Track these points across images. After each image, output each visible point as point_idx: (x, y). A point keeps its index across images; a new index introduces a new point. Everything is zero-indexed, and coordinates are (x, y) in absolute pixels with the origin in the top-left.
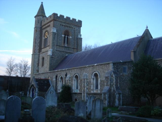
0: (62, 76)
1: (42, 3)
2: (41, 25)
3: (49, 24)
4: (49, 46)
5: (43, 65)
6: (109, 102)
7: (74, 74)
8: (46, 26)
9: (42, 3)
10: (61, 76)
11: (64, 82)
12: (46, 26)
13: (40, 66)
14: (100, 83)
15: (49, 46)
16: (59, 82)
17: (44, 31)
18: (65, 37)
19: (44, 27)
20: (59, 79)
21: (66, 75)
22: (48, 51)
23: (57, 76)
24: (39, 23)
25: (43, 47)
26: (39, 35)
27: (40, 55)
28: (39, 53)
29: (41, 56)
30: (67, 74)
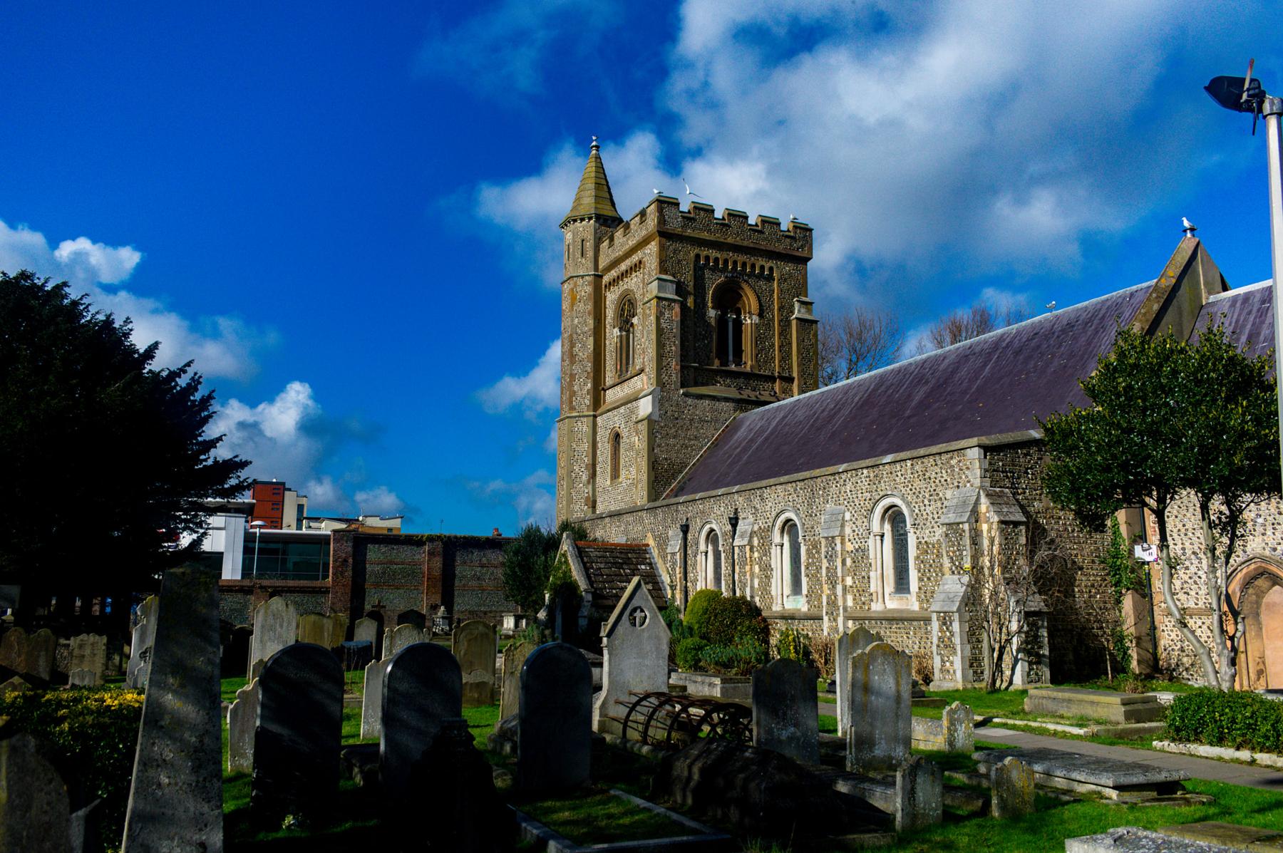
0: (714, 526)
2: (596, 268)
3: (635, 258)
4: (642, 371)
5: (615, 475)
6: (971, 666)
7: (774, 514)
8: (623, 267)
10: (707, 528)
11: (727, 558)
12: (623, 267)
13: (603, 480)
15: (642, 371)
17: (611, 297)
18: (722, 321)
19: (614, 273)
21: (734, 522)
22: (636, 399)
23: (685, 529)
25: (610, 378)
27: (599, 419)
28: (595, 410)
29: (606, 423)
30: (741, 515)
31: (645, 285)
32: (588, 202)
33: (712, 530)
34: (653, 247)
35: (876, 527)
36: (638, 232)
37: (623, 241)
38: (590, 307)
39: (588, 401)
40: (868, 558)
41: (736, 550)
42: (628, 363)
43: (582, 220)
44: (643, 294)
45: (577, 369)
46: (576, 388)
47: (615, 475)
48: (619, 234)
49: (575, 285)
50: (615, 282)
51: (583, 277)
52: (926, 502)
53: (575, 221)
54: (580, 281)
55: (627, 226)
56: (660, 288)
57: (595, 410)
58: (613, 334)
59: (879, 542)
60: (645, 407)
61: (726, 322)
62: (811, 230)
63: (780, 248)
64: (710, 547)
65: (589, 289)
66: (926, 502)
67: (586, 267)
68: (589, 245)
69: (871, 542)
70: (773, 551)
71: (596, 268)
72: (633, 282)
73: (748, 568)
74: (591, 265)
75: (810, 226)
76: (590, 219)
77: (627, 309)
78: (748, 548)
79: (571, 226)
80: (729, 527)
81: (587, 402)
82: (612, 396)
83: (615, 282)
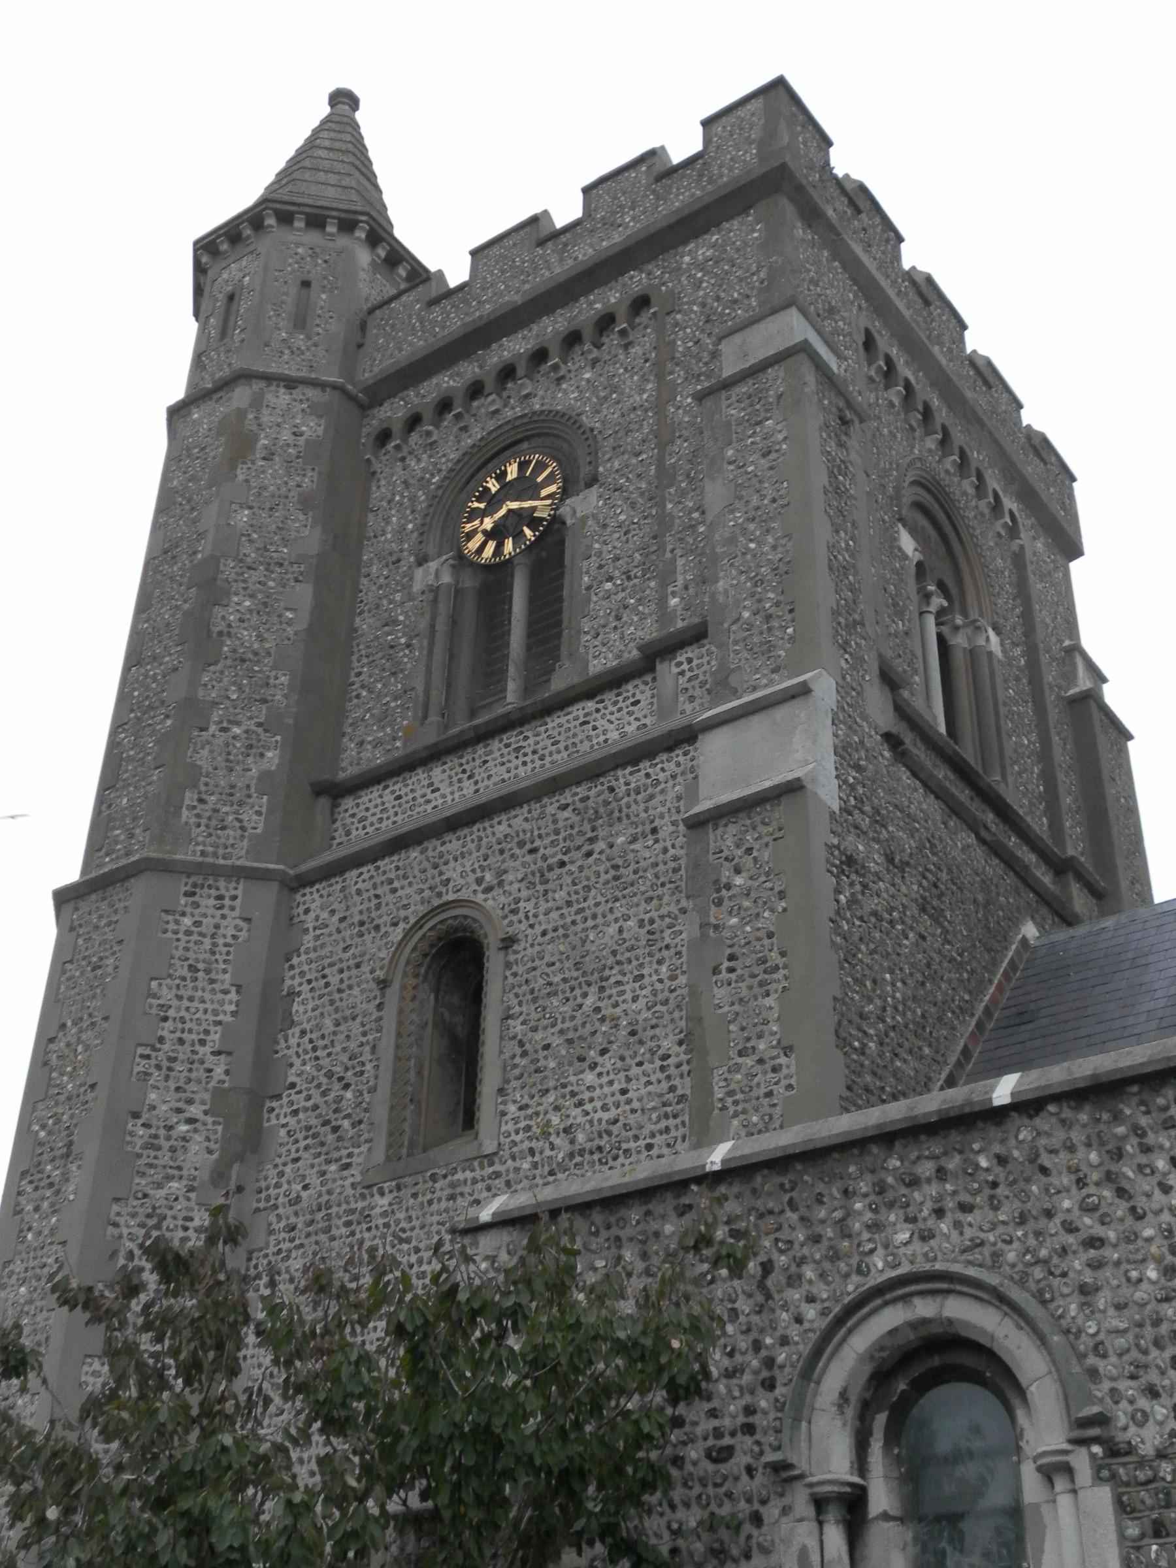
1: (344, 101)
9: (344, 101)
24: (300, 321)
26: (308, 535)
51: (291, 383)
54: (282, 398)
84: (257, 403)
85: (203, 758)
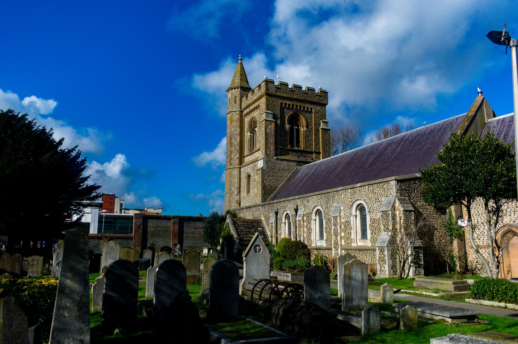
0: (288, 212)
2: (241, 108)
3: (256, 104)
4: (259, 149)
5: (248, 191)
6: (392, 268)
7: (312, 207)
10: (316, 209)
13: (244, 194)
14: (370, 225)
16: (283, 225)
17: (247, 120)
18: (291, 129)
20: (281, 219)
21: (296, 210)
22: (257, 161)
23: (277, 213)
25: (246, 152)
27: (242, 169)
28: (240, 165)
29: (245, 170)
30: (299, 208)
31: (261, 115)
32: (237, 82)
33: (287, 214)
34: (264, 100)
35: (354, 212)
36: (258, 94)
37: (251, 97)
38: (238, 124)
39: (237, 162)
40: (350, 225)
41: (297, 222)
42: (253, 146)
43: (235, 89)
44: (260, 119)
45: (233, 149)
46: (232, 156)
47: (248, 191)
48: (250, 94)
49: (232, 115)
50: (248, 114)
51: (235, 112)
52: (374, 202)
53: (232, 89)
54: (234, 113)
55: (253, 91)
56: (266, 116)
57: (240, 165)
58: (247, 135)
59: (355, 218)
60: (260, 164)
61: (293, 130)
62: (327, 93)
63: (315, 100)
64: (287, 221)
65: (238, 116)
66: (374, 202)
67: (236, 108)
68: (238, 99)
69: (352, 218)
70: (312, 222)
71: (241, 108)
72: (255, 114)
73: (302, 229)
74: (238, 107)
75: (327, 91)
76: (238, 88)
77: (253, 125)
78: (302, 221)
79: (231, 91)
80: (294, 213)
81: (237, 162)
82: (247, 160)
83: (248, 114)
84: (232, 115)
85: (232, 156)
